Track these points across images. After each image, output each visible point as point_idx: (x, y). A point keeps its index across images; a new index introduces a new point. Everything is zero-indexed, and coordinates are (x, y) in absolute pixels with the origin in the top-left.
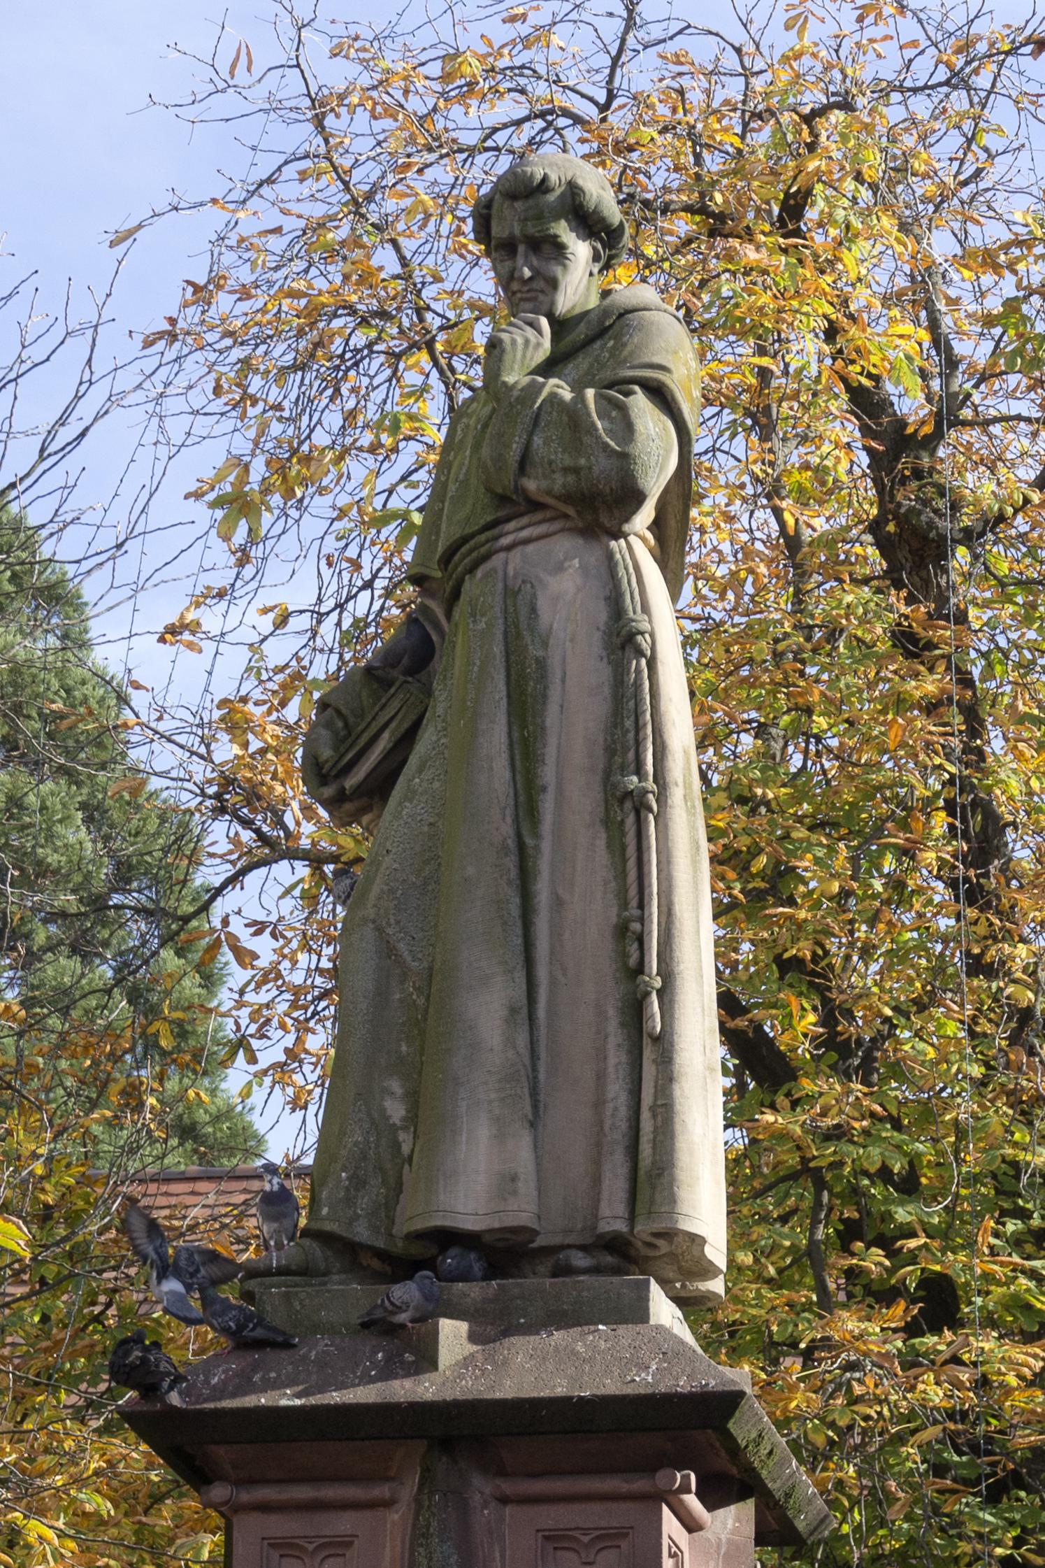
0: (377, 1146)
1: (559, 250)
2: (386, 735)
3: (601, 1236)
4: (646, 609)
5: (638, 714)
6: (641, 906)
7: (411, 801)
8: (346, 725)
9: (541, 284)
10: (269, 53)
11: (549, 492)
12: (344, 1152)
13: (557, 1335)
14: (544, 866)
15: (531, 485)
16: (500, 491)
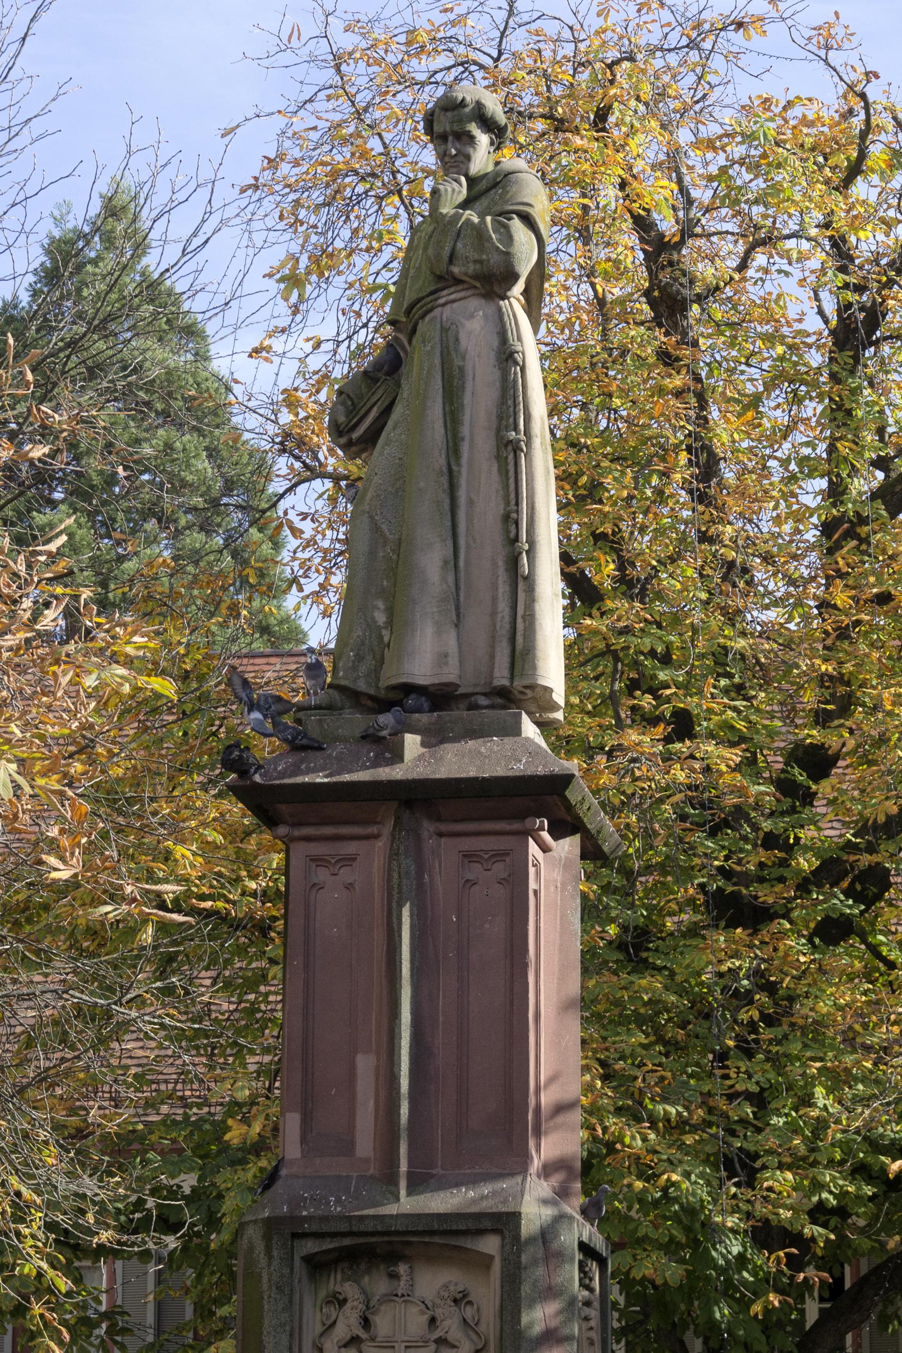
1: (471, 139)
4: (520, 339)
5: (515, 398)
6: (517, 504)
9: (461, 158)
10: (310, 29)
11: (466, 274)
15: (456, 270)
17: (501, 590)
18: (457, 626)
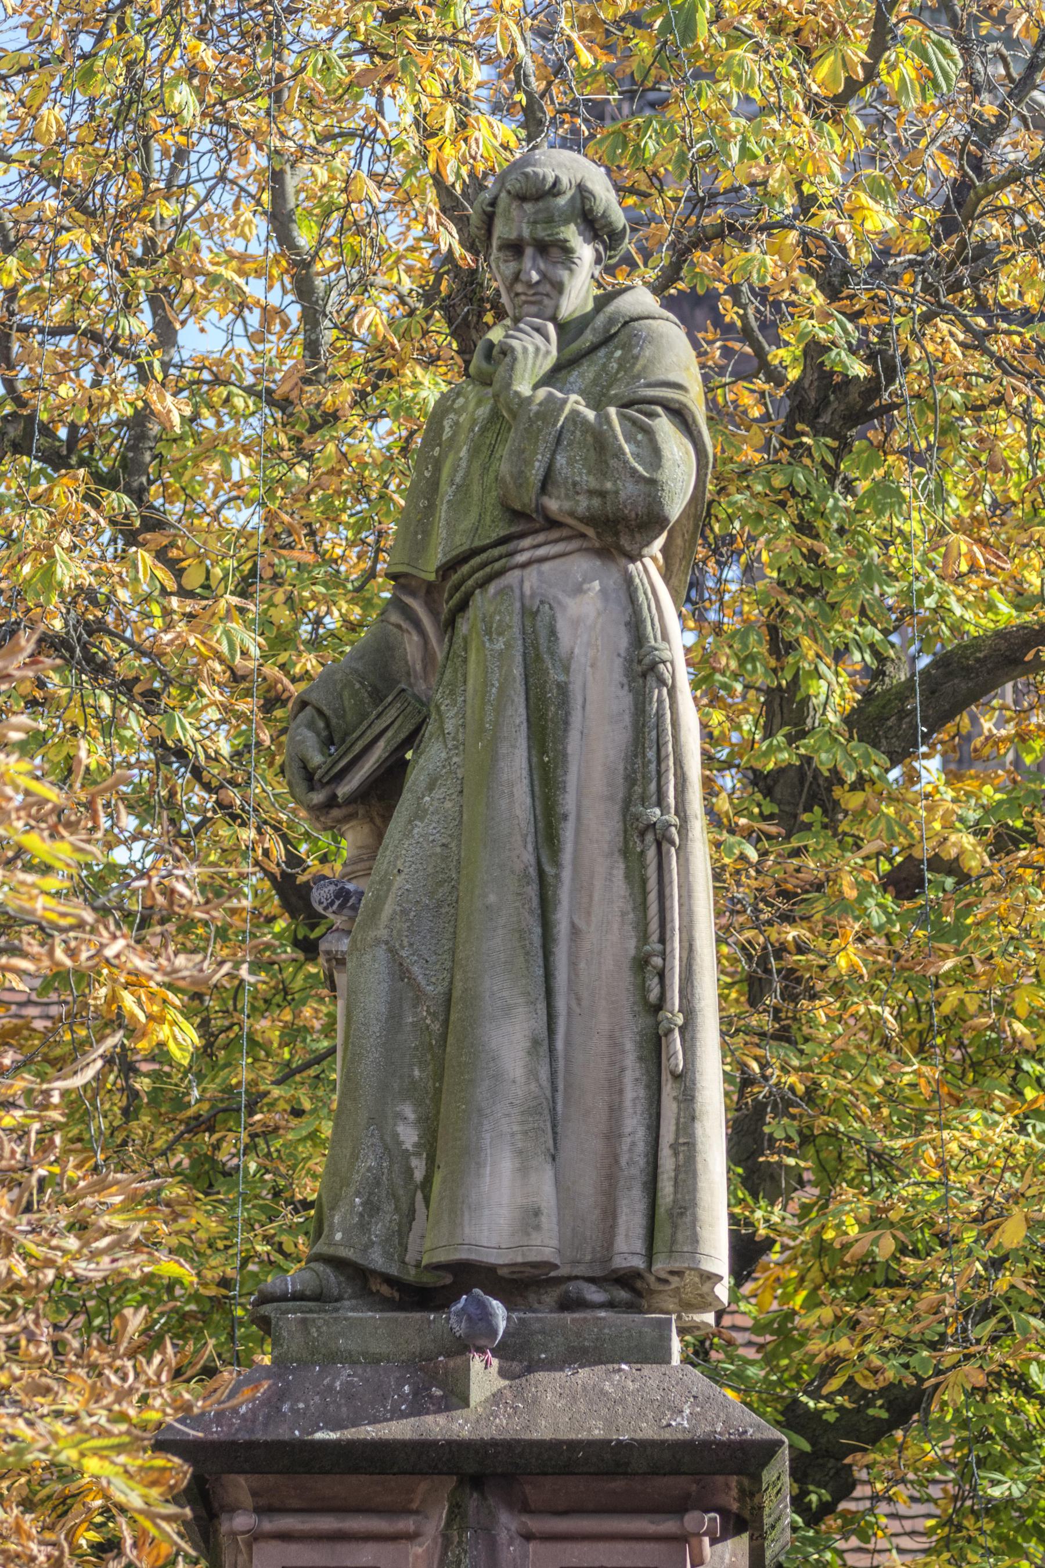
0: (390, 1171)
1: (567, 251)
2: (381, 744)
3: (614, 1271)
4: (665, 637)
6: (662, 940)
7: (422, 820)
8: (328, 725)
9: (547, 288)
11: (572, 514)
12: (357, 1177)
13: (584, 1373)
14: (564, 895)
15: (553, 505)
16: (518, 506)
17: (629, 1094)
18: (554, 1158)
